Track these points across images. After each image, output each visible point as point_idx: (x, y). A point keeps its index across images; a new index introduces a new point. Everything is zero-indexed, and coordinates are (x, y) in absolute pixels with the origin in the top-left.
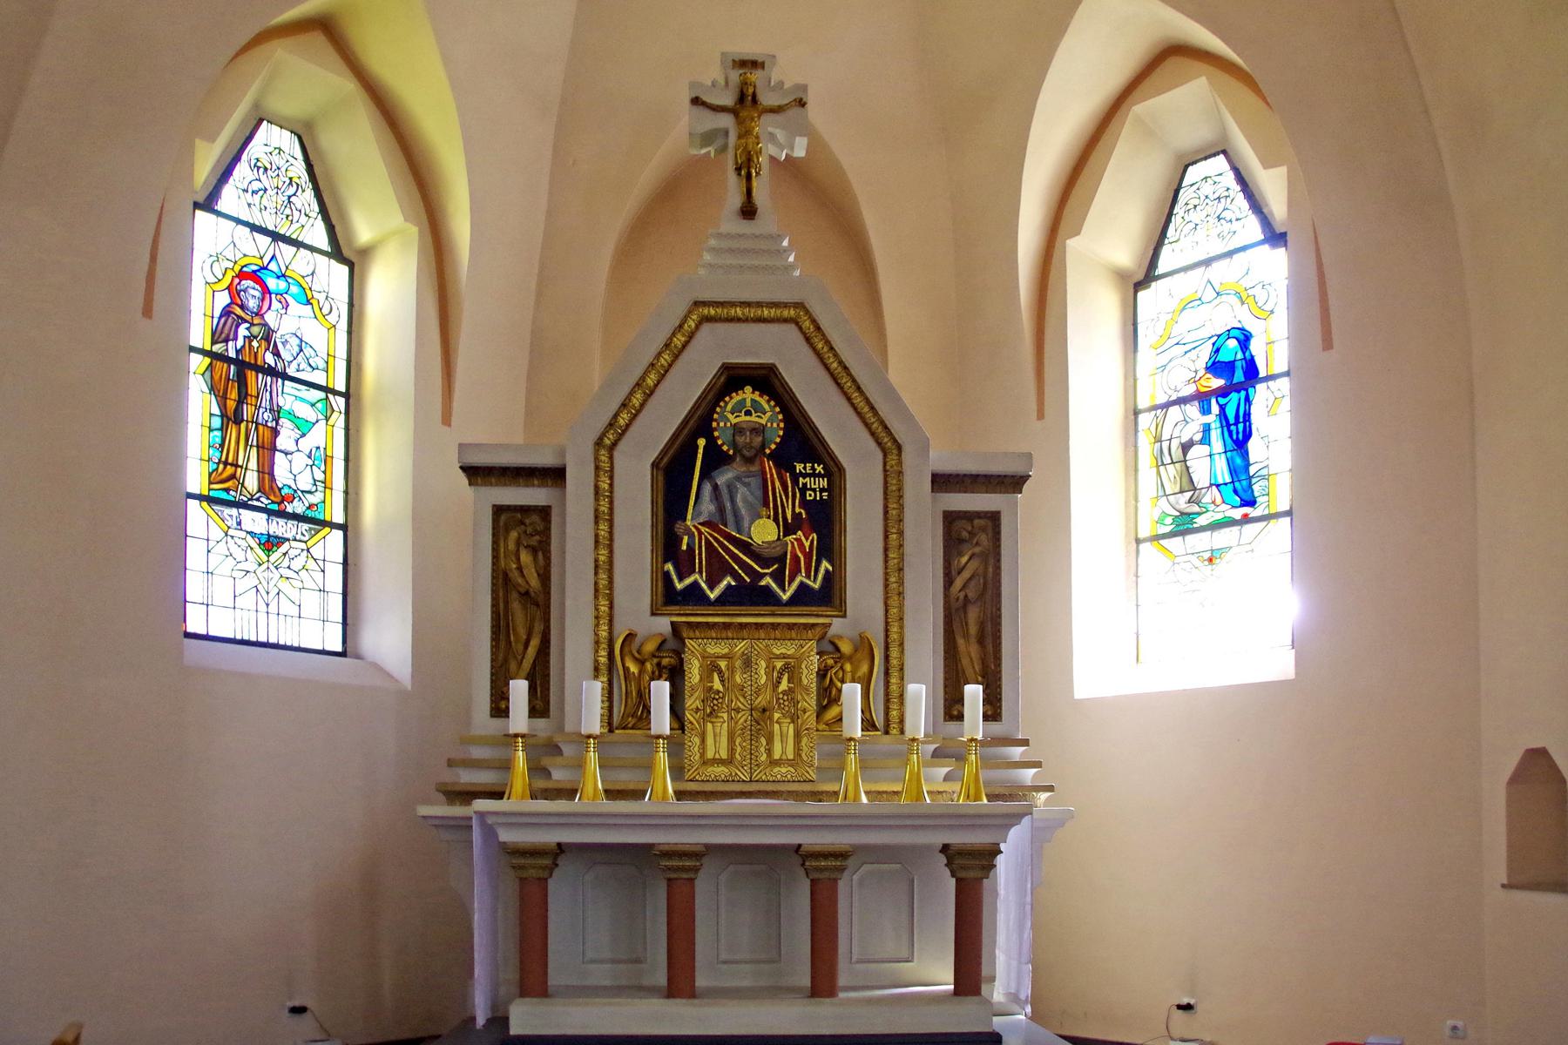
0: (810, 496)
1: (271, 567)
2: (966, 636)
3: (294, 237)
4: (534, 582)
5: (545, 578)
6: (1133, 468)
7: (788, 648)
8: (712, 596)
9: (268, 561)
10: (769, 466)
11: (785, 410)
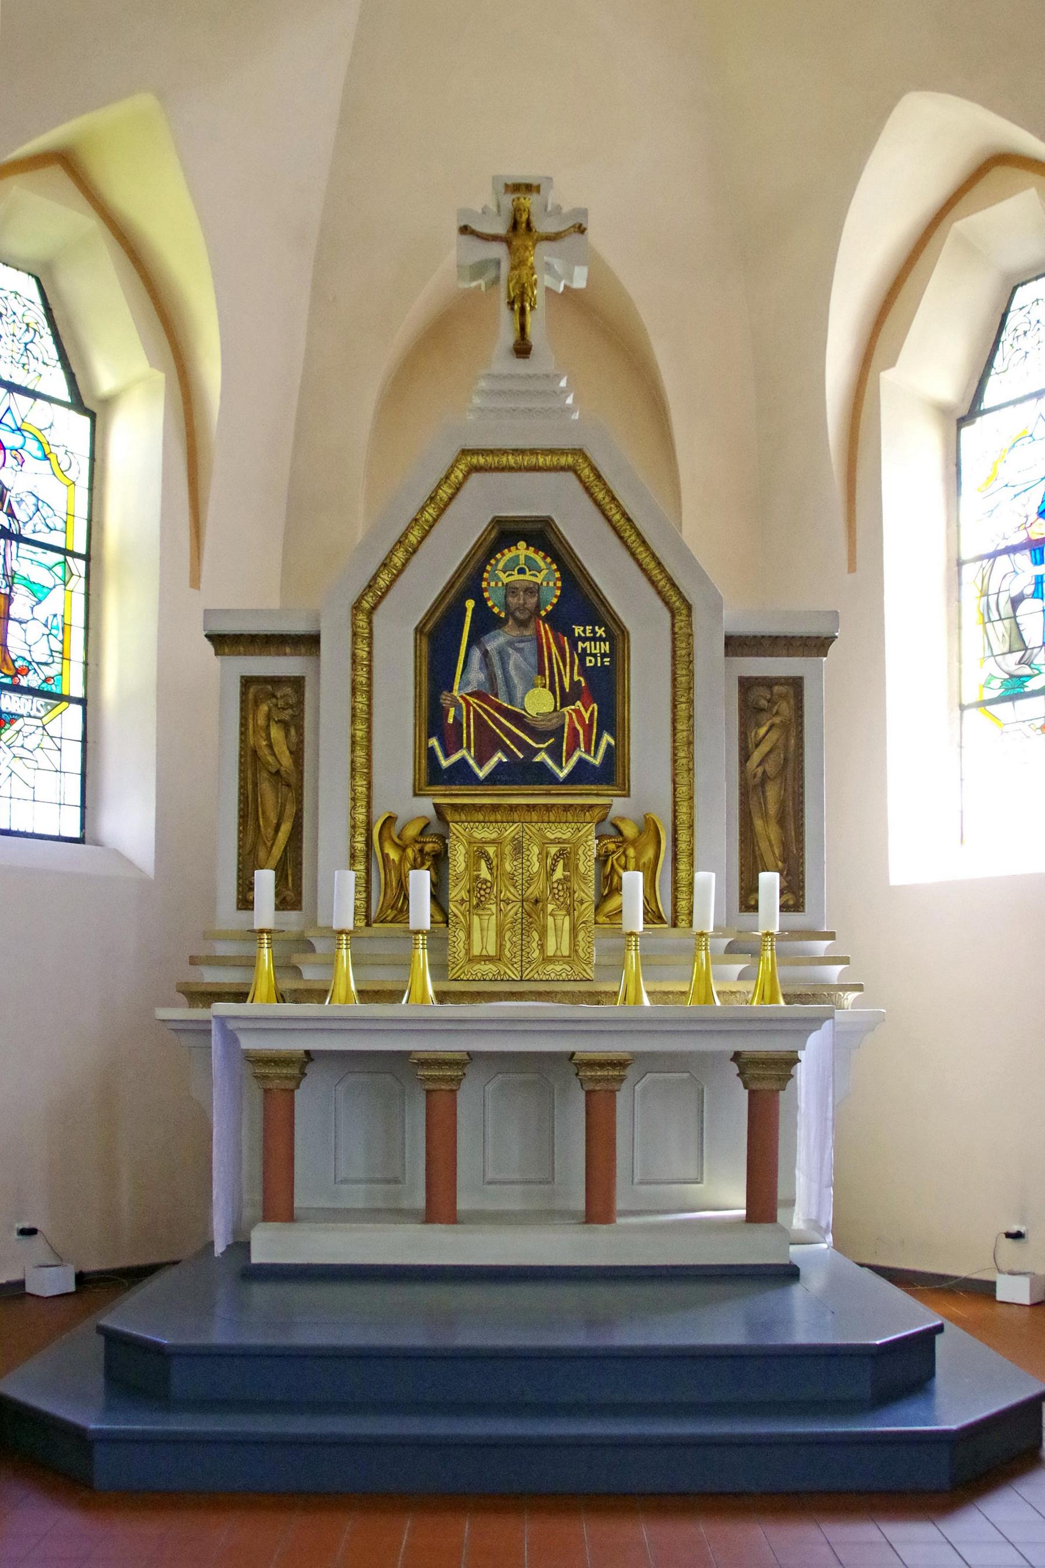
0: (590, 662)
2: (765, 816)
4: (286, 760)
5: (297, 754)
6: (956, 626)
7: (563, 832)
8: (482, 774)
10: (545, 629)
11: (562, 568)
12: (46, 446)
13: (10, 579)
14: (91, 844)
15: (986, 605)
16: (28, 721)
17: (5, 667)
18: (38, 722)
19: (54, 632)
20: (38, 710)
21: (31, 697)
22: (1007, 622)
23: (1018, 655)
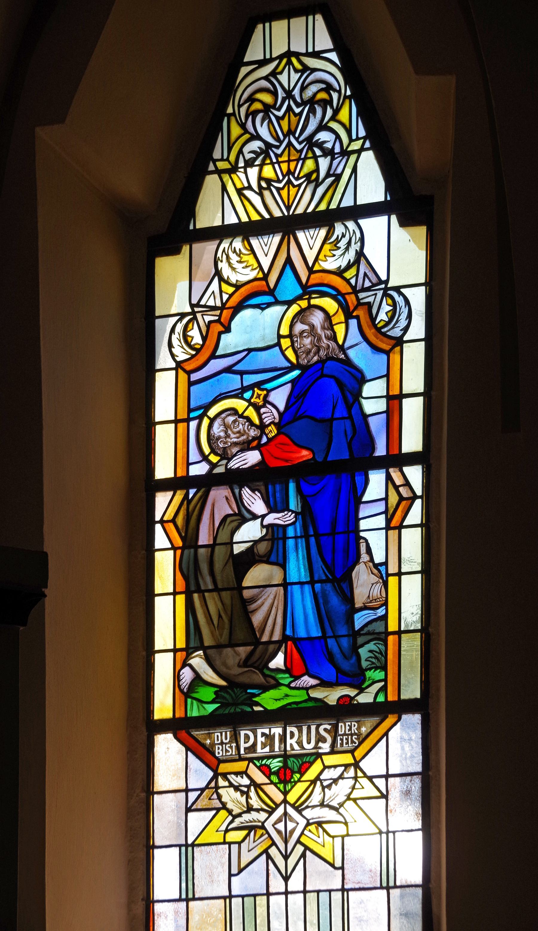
1: (290, 810)
3: (348, 202)
9: (285, 801)
12: (351, 300)
15: (192, 563)
18: (348, 759)
22: (225, 595)
23: (243, 651)
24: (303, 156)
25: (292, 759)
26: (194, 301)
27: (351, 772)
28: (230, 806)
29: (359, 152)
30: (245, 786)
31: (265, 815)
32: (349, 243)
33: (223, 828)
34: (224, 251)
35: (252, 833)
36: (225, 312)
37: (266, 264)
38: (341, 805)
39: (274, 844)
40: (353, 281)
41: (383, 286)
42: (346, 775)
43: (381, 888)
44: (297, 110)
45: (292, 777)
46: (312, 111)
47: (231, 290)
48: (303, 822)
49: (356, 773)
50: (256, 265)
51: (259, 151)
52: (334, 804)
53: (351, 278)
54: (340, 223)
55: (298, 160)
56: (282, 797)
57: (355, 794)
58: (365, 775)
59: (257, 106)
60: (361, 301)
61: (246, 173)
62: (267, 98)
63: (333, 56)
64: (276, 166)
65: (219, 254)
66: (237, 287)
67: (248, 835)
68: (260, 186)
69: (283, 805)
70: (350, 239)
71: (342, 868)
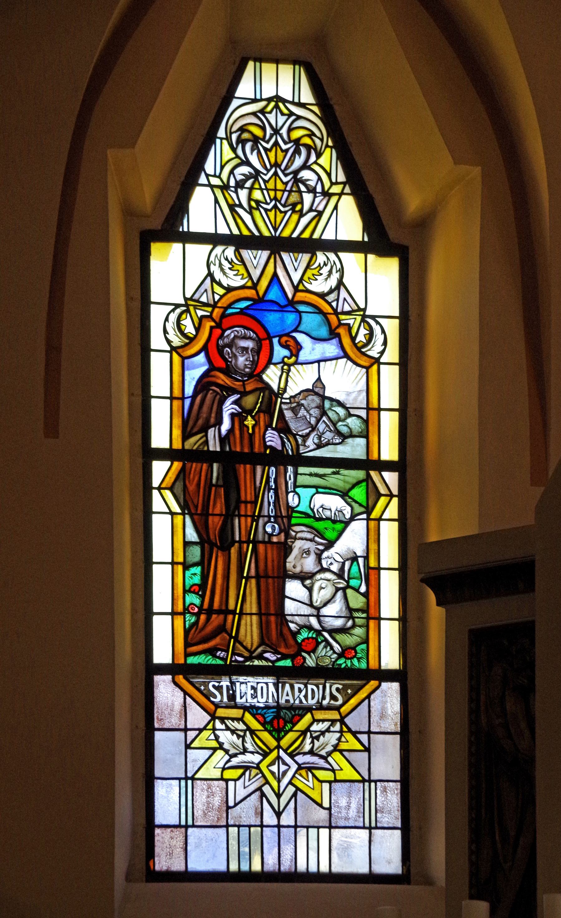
9: (278, 747)
12: (333, 318)
13: (285, 520)
14: (418, 883)
16: (319, 715)
17: (283, 644)
18: (335, 715)
19: (353, 583)
20: (333, 697)
21: (322, 681)
24: (288, 188)
25: (284, 711)
26: (188, 295)
27: (337, 727)
28: (226, 746)
29: (340, 195)
30: (241, 730)
31: (260, 757)
32: (330, 272)
33: (221, 765)
34: (216, 256)
35: (247, 773)
36: (217, 310)
37: (255, 274)
38: (329, 754)
39: (267, 782)
40: (334, 304)
41: (362, 313)
42: (332, 729)
43: (364, 828)
44: (284, 147)
45: (284, 727)
46: (297, 152)
47: (221, 291)
48: (294, 767)
49: (341, 728)
50: (246, 275)
51: (249, 174)
52: (323, 753)
53: (333, 301)
54: (322, 253)
55: (284, 191)
56: (275, 743)
57: (343, 746)
58: (350, 730)
59: (246, 136)
60: (342, 322)
61: (236, 192)
62: (258, 132)
63: (315, 109)
64: (265, 192)
65: (212, 258)
66: (229, 289)
67: (243, 774)
68: (250, 207)
69: (276, 750)
70: (332, 267)
71: (330, 809)
